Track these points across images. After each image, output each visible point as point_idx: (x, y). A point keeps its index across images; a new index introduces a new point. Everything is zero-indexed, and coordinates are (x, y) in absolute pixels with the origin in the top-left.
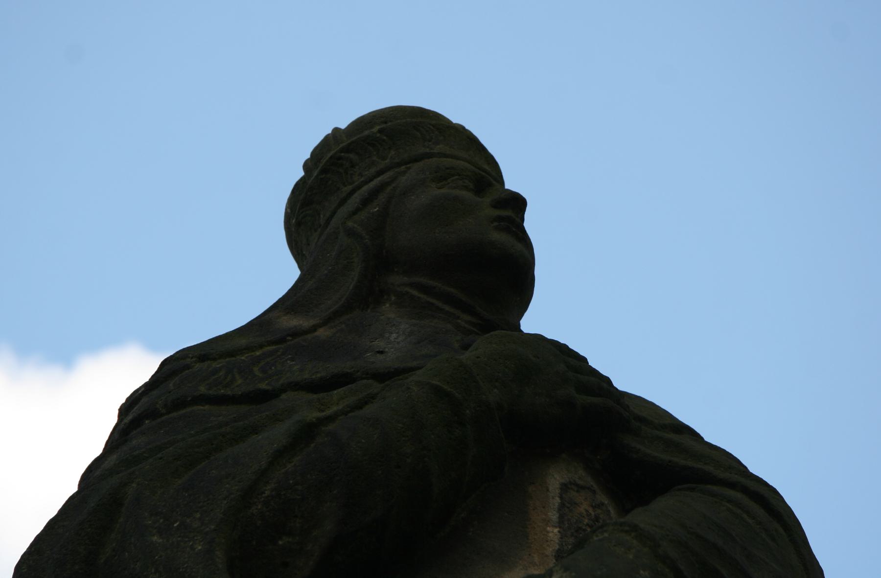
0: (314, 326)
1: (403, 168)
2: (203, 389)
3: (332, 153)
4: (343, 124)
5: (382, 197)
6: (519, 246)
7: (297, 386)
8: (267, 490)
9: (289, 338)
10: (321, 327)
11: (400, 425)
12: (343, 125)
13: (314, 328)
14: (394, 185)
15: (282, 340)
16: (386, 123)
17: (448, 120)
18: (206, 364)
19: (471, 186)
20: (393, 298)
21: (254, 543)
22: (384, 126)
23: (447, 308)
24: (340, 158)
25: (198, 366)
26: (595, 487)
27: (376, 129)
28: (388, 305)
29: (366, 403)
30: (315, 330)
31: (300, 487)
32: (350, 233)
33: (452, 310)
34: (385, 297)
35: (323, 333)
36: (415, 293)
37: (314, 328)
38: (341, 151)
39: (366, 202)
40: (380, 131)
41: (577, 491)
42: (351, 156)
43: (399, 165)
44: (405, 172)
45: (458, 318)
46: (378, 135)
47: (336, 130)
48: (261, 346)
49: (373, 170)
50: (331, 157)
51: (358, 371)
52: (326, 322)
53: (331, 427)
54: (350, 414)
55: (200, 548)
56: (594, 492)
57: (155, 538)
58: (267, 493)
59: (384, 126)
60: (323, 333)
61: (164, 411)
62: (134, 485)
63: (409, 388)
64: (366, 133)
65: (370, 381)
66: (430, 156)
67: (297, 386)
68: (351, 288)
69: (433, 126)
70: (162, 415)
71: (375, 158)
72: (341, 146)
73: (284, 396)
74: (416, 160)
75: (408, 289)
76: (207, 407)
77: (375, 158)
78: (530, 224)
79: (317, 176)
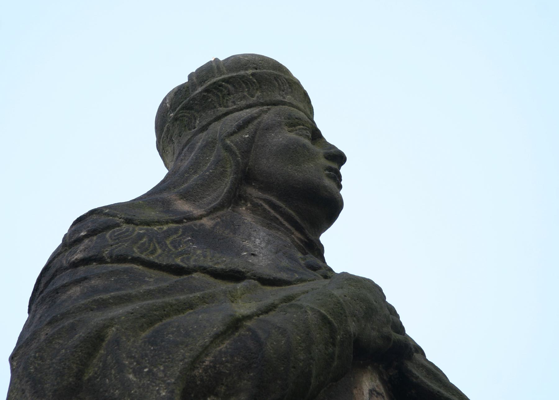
0: (201, 215)
1: (265, 108)
2: (136, 252)
3: (215, 80)
4: (222, 58)
5: (251, 127)
6: (328, 183)
7: (204, 270)
8: (208, 361)
9: (185, 221)
10: (205, 217)
11: (298, 337)
12: (222, 58)
13: (201, 217)
14: (259, 120)
15: (179, 222)
16: (256, 69)
17: (275, 61)
18: (131, 226)
19: (310, 135)
20: (249, 205)
21: (193, 395)
22: (255, 71)
23: (287, 224)
24: (221, 86)
25: (125, 227)
26: (384, 394)
27: (250, 72)
28: (244, 209)
29: (271, 310)
30: (201, 219)
31: (229, 365)
32: (227, 148)
33: (289, 227)
34: (243, 202)
35: (207, 222)
36: (267, 207)
37: (201, 217)
38: (224, 80)
39: (241, 128)
40: (253, 75)
41: (377, 397)
42: (229, 86)
43: (262, 104)
44: (266, 112)
45: (293, 234)
46: (251, 77)
47: (216, 60)
48: (167, 223)
49: (243, 103)
50: (215, 83)
51: (248, 272)
52: (210, 213)
53: (249, 324)
54: (261, 316)
55: (164, 394)
56: (383, 397)
57: (131, 376)
58: (207, 363)
59: (255, 71)
60: (207, 222)
61: (109, 260)
62: (113, 329)
63: (306, 312)
64: (242, 73)
65: (256, 282)
66: (283, 103)
67: (204, 270)
68: (225, 190)
69: (286, 80)
70: (107, 263)
71: (246, 94)
72: (223, 77)
73: (194, 275)
74: (275, 104)
75: (261, 202)
76: (140, 267)
77: (246, 94)
78: (343, 170)
79: (200, 93)
